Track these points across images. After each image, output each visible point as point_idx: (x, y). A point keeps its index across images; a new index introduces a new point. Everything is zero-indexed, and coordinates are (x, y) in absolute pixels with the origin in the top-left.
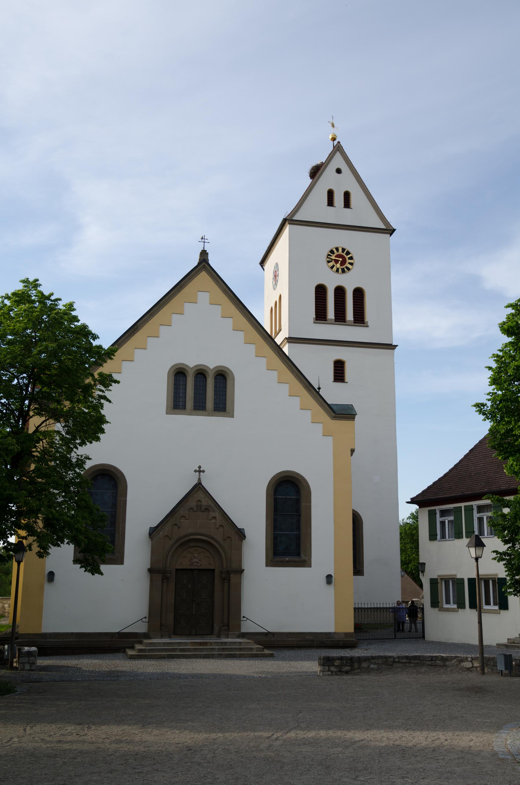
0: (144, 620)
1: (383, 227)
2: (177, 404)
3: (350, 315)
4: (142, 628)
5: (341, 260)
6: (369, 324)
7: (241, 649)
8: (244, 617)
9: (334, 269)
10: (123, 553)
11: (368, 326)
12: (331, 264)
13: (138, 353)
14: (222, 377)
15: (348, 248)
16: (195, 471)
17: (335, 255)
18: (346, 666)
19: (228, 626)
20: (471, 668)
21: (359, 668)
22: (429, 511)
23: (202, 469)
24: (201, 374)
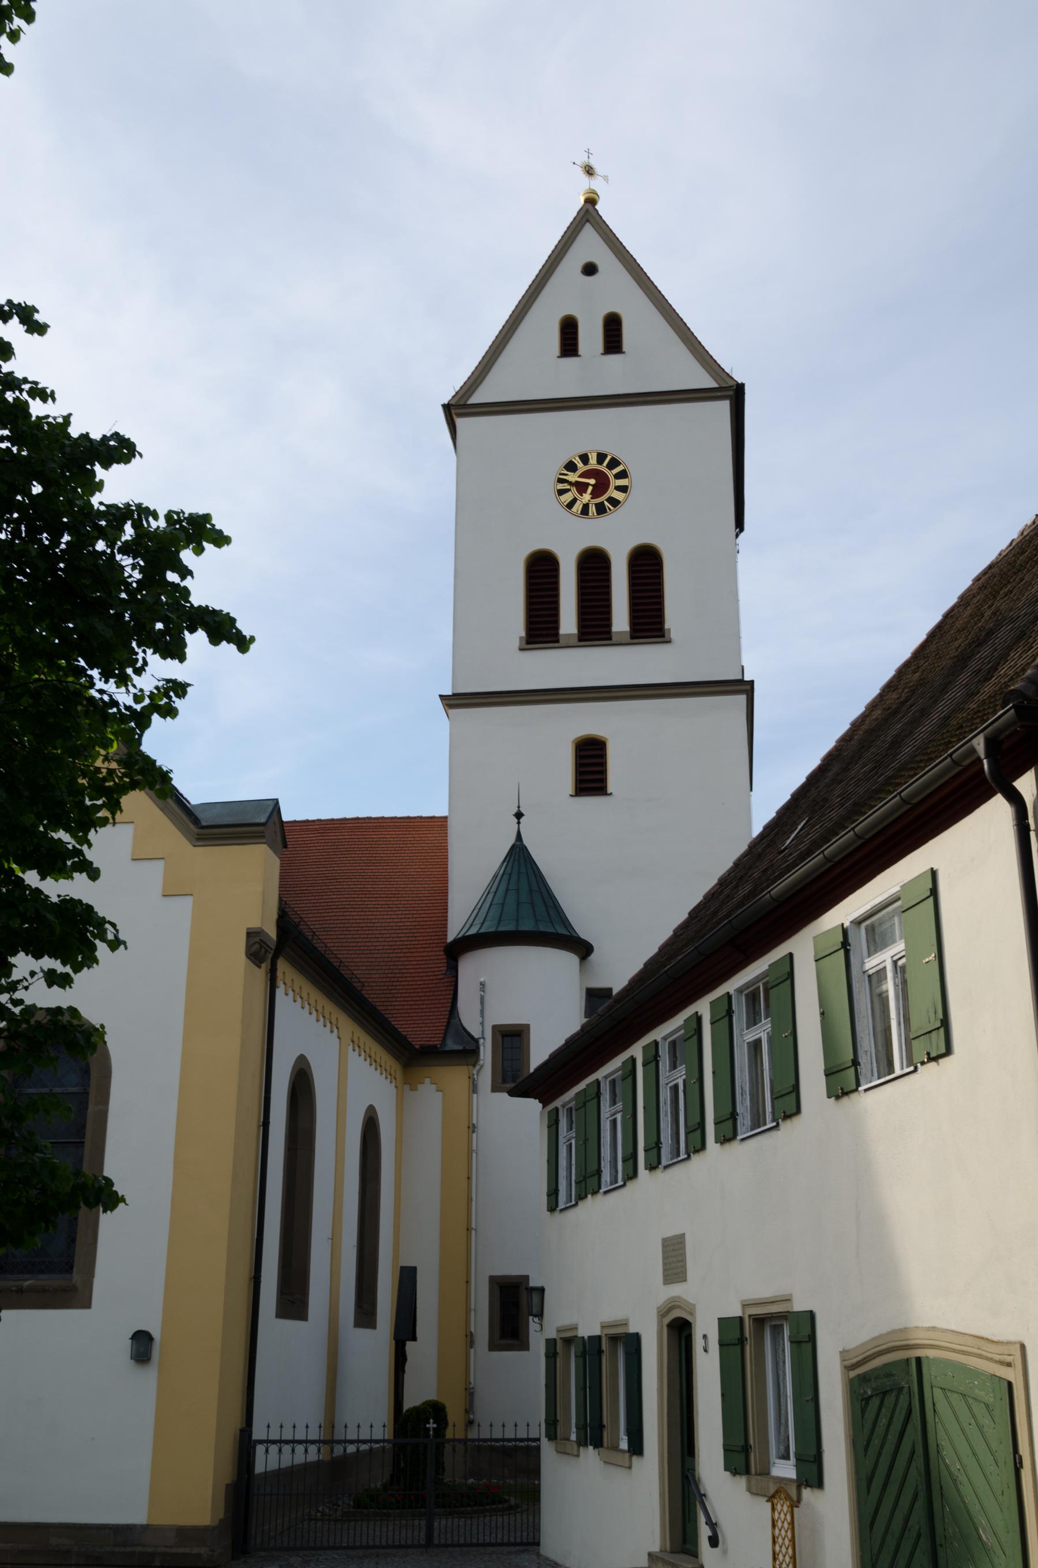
1: (710, 383)
5: (597, 482)
9: (574, 509)
11: (669, 642)
12: (567, 498)
15: (612, 451)
17: (579, 472)
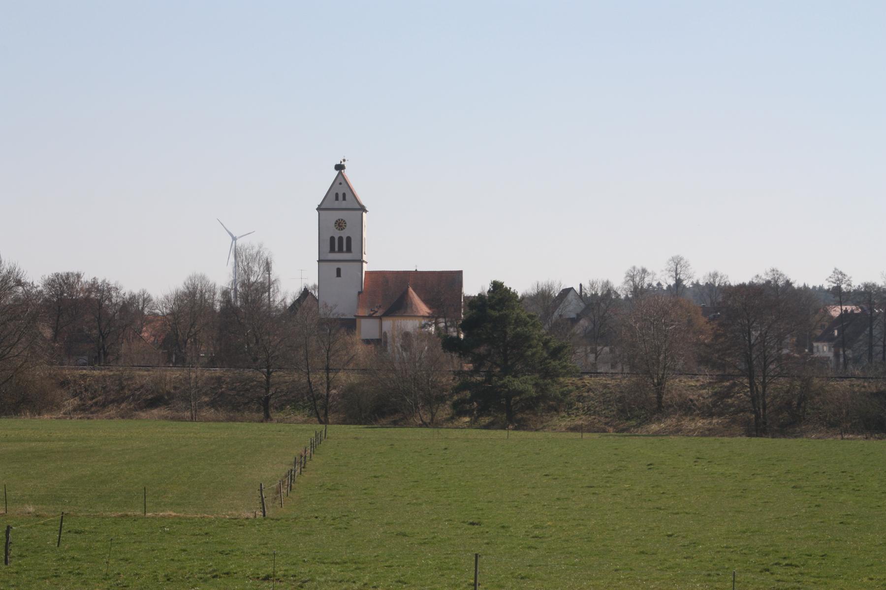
3: (345, 249)
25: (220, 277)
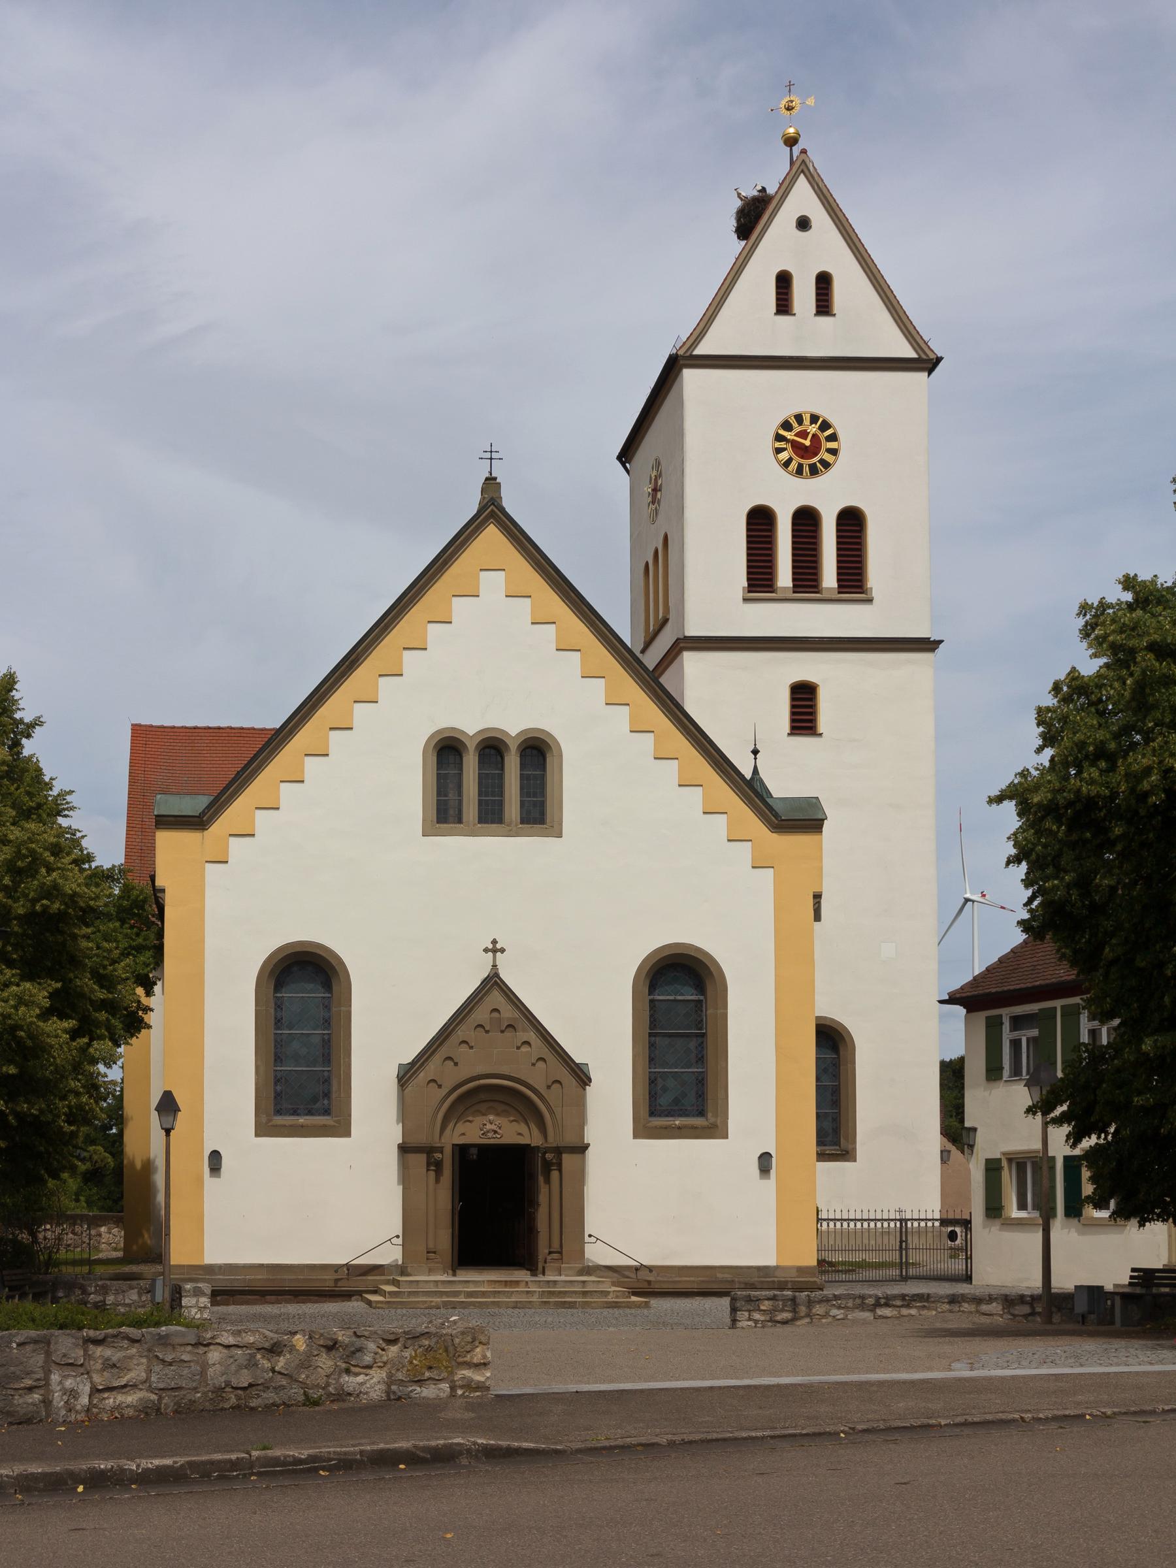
0: (395, 1241)
2: (445, 813)
3: (784, 576)
4: (392, 1255)
6: (874, 594)
7: (585, 1294)
8: (590, 1236)
9: (790, 468)
10: (350, 1116)
13: (361, 711)
14: (537, 751)
16: (486, 950)
18: (782, 1310)
19: (560, 1253)
20: (1030, 1315)
21: (808, 1315)
22: (987, 1018)
23: (498, 946)
24: (492, 748)
25: (1009, 817)
